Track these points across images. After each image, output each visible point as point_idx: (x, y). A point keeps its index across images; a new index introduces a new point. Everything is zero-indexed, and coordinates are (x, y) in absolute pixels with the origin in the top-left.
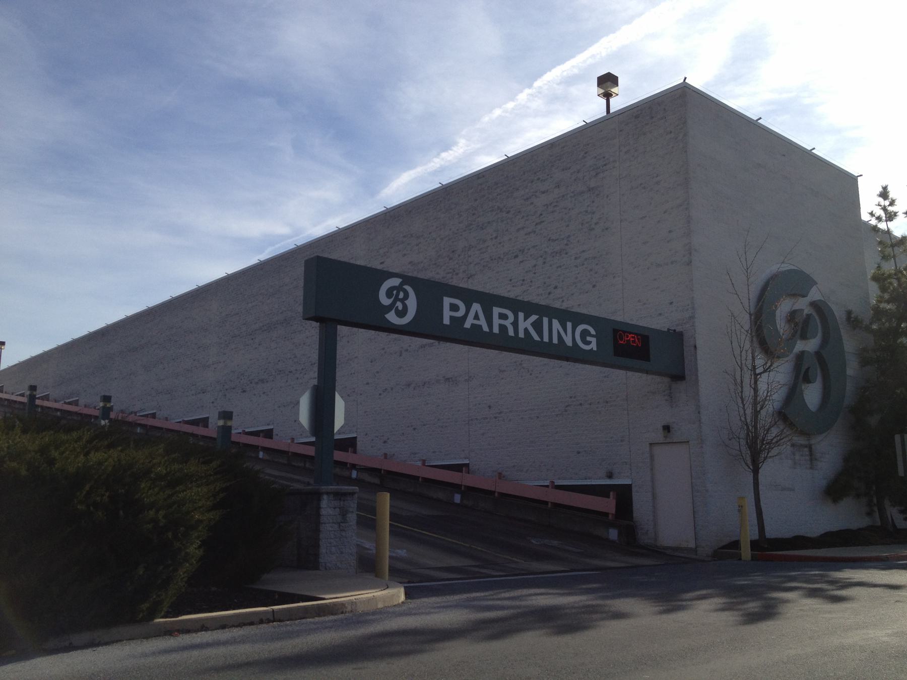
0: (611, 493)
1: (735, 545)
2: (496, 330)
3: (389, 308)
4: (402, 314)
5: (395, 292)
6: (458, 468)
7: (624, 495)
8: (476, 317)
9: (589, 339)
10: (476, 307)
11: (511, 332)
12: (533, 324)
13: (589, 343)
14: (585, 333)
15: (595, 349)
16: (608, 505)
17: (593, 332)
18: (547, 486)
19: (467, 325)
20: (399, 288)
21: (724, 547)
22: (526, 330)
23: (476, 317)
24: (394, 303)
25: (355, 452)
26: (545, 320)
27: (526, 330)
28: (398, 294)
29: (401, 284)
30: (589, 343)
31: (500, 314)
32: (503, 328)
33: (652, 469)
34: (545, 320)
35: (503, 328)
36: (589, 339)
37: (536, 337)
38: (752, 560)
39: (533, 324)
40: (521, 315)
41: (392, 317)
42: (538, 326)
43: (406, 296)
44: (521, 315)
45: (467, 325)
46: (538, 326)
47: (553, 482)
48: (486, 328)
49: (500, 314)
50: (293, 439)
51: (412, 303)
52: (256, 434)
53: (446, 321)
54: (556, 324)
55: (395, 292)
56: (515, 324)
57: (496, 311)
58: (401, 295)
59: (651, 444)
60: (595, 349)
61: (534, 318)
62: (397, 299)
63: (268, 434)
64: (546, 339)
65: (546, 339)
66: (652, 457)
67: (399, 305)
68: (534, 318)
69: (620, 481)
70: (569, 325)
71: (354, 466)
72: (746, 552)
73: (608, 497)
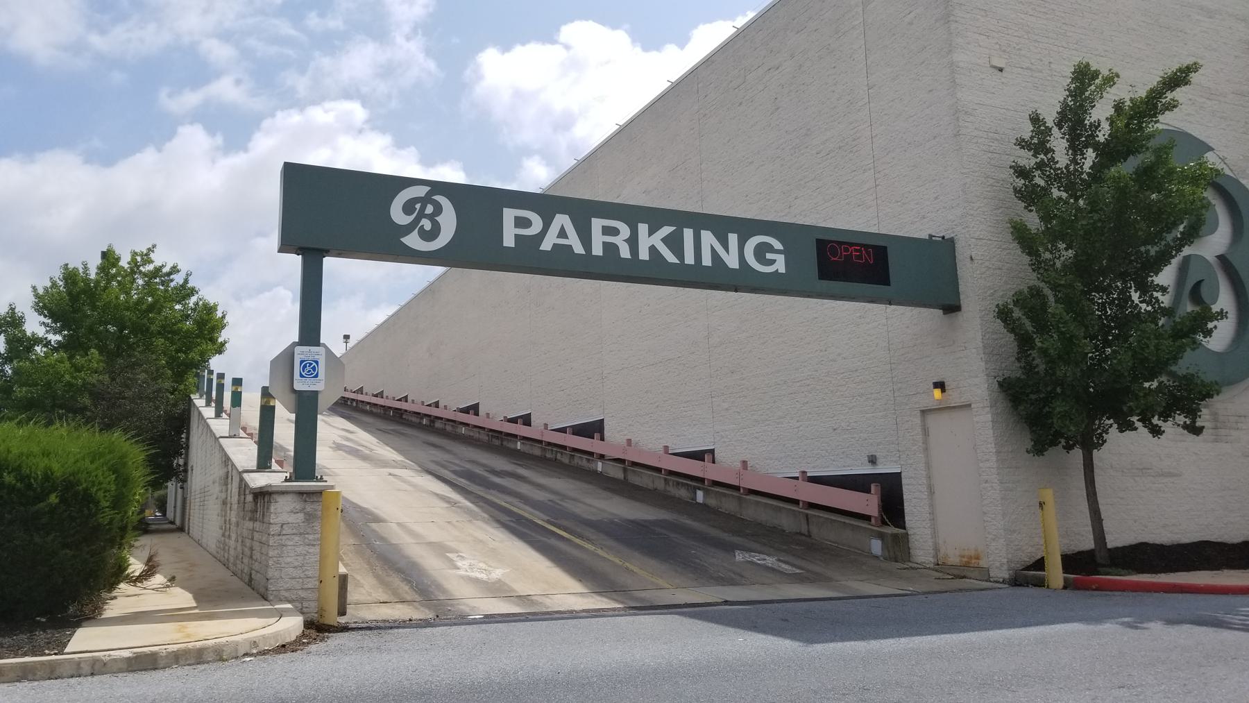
0: (873, 486)
1: (1040, 564)
2: (597, 250)
3: (408, 229)
4: (430, 236)
5: (418, 206)
6: (698, 456)
7: (891, 492)
8: (562, 233)
9: (769, 256)
10: (562, 220)
11: (625, 253)
12: (665, 240)
13: (772, 262)
14: (761, 251)
15: (782, 270)
16: (868, 503)
17: (777, 245)
18: (797, 478)
19: (546, 246)
20: (425, 200)
21: (1028, 568)
22: (653, 249)
23: (562, 233)
24: (417, 220)
25: (602, 439)
26: (688, 234)
27: (653, 249)
28: (423, 208)
29: (429, 194)
30: (772, 262)
31: (516, 218)
32: (610, 249)
33: (926, 449)
34: (688, 234)
35: (610, 249)
36: (769, 256)
37: (671, 258)
38: (1065, 588)
39: (665, 240)
40: (643, 228)
41: (413, 241)
42: (674, 243)
43: (438, 209)
44: (643, 228)
45: (546, 246)
46: (674, 243)
47: (666, 448)
48: (579, 249)
49: (516, 218)
50: (546, 425)
51: (448, 221)
52: (513, 421)
53: (509, 241)
54: (708, 238)
55: (418, 206)
56: (633, 242)
57: (597, 224)
58: (429, 209)
59: (923, 412)
60: (782, 270)
61: (666, 230)
62: (422, 214)
63: (526, 420)
64: (689, 259)
65: (689, 259)
66: (926, 432)
67: (426, 224)
68: (666, 230)
69: (885, 467)
70: (733, 238)
71: (602, 457)
72: (1055, 573)
73: (868, 491)
